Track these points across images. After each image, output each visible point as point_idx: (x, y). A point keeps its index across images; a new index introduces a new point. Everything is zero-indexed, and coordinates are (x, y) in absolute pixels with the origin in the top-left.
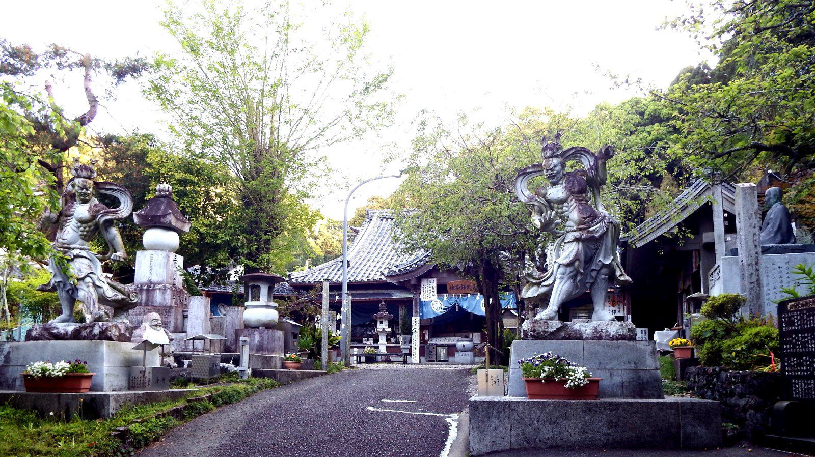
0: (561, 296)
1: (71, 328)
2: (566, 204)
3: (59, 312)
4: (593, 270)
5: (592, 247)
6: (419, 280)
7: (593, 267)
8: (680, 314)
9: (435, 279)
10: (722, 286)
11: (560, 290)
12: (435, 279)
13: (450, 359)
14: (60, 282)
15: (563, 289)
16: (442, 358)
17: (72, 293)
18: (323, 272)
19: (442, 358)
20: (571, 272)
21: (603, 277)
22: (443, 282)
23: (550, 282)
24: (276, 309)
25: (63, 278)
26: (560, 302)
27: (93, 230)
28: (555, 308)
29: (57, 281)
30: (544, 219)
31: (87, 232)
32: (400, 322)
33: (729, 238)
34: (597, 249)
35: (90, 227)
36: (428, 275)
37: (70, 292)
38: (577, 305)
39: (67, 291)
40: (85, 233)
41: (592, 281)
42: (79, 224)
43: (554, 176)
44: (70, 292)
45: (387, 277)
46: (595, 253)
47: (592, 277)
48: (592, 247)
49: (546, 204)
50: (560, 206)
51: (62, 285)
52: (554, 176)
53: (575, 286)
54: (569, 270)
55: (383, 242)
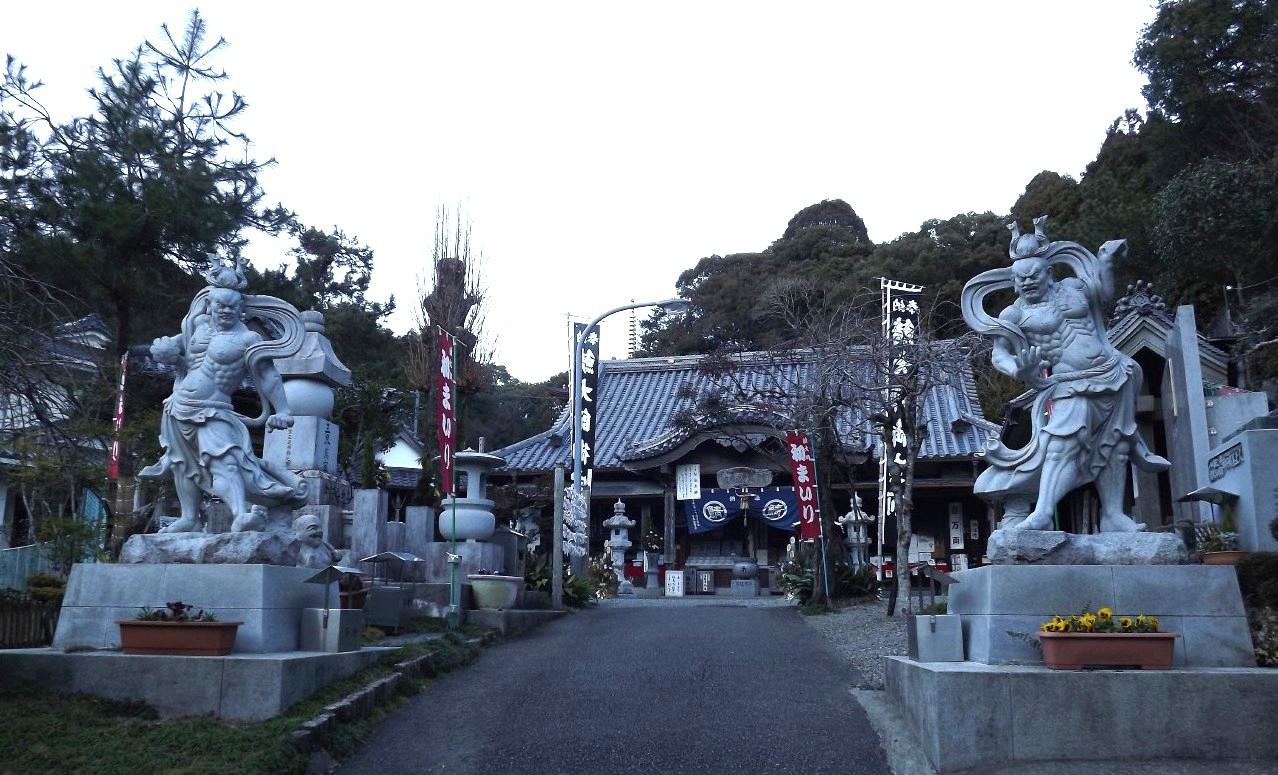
0: (1058, 489)
1: (199, 542)
2: (1056, 334)
3: (175, 512)
4: (1105, 445)
5: (1104, 406)
6: (673, 467)
7: (1104, 442)
8: (1073, 521)
9: (698, 466)
10: (1250, 477)
11: (1053, 482)
12: (698, 466)
13: (721, 590)
14: (180, 462)
15: (1061, 476)
16: (705, 588)
17: (200, 482)
18: (520, 453)
19: (705, 588)
20: (1073, 449)
21: (1121, 457)
22: (710, 470)
23: (1031, 466)
24: (493, 510)
25: (185, 455)
26: (1057, 499)
27: (239, 374)
28: (1050, 510)
29: (175, 460)
30: (1026, 360)
31: (229, 378)
32: (31, 519)
33: (1211, 403)
34: (1112, 411)
35: (234, 370)
36: (688, 460)
37: (197, 480)
38: (1078, 509)
39: (192, 479)
40: (225, 380)
41: (1102, 465)
42: (216, 365)
43: (1035, 288)
44: (197, 480)
45: (625, 462)
46: (1108, 419)
47: (1103, 458)
48: (1104, 406)
49: (1020, 333)
50: (1047, 337)
51: (183, 468)
52: (1035, 288)
53: (1079, 472)
54: (1069, 444)
55: (618, 410)
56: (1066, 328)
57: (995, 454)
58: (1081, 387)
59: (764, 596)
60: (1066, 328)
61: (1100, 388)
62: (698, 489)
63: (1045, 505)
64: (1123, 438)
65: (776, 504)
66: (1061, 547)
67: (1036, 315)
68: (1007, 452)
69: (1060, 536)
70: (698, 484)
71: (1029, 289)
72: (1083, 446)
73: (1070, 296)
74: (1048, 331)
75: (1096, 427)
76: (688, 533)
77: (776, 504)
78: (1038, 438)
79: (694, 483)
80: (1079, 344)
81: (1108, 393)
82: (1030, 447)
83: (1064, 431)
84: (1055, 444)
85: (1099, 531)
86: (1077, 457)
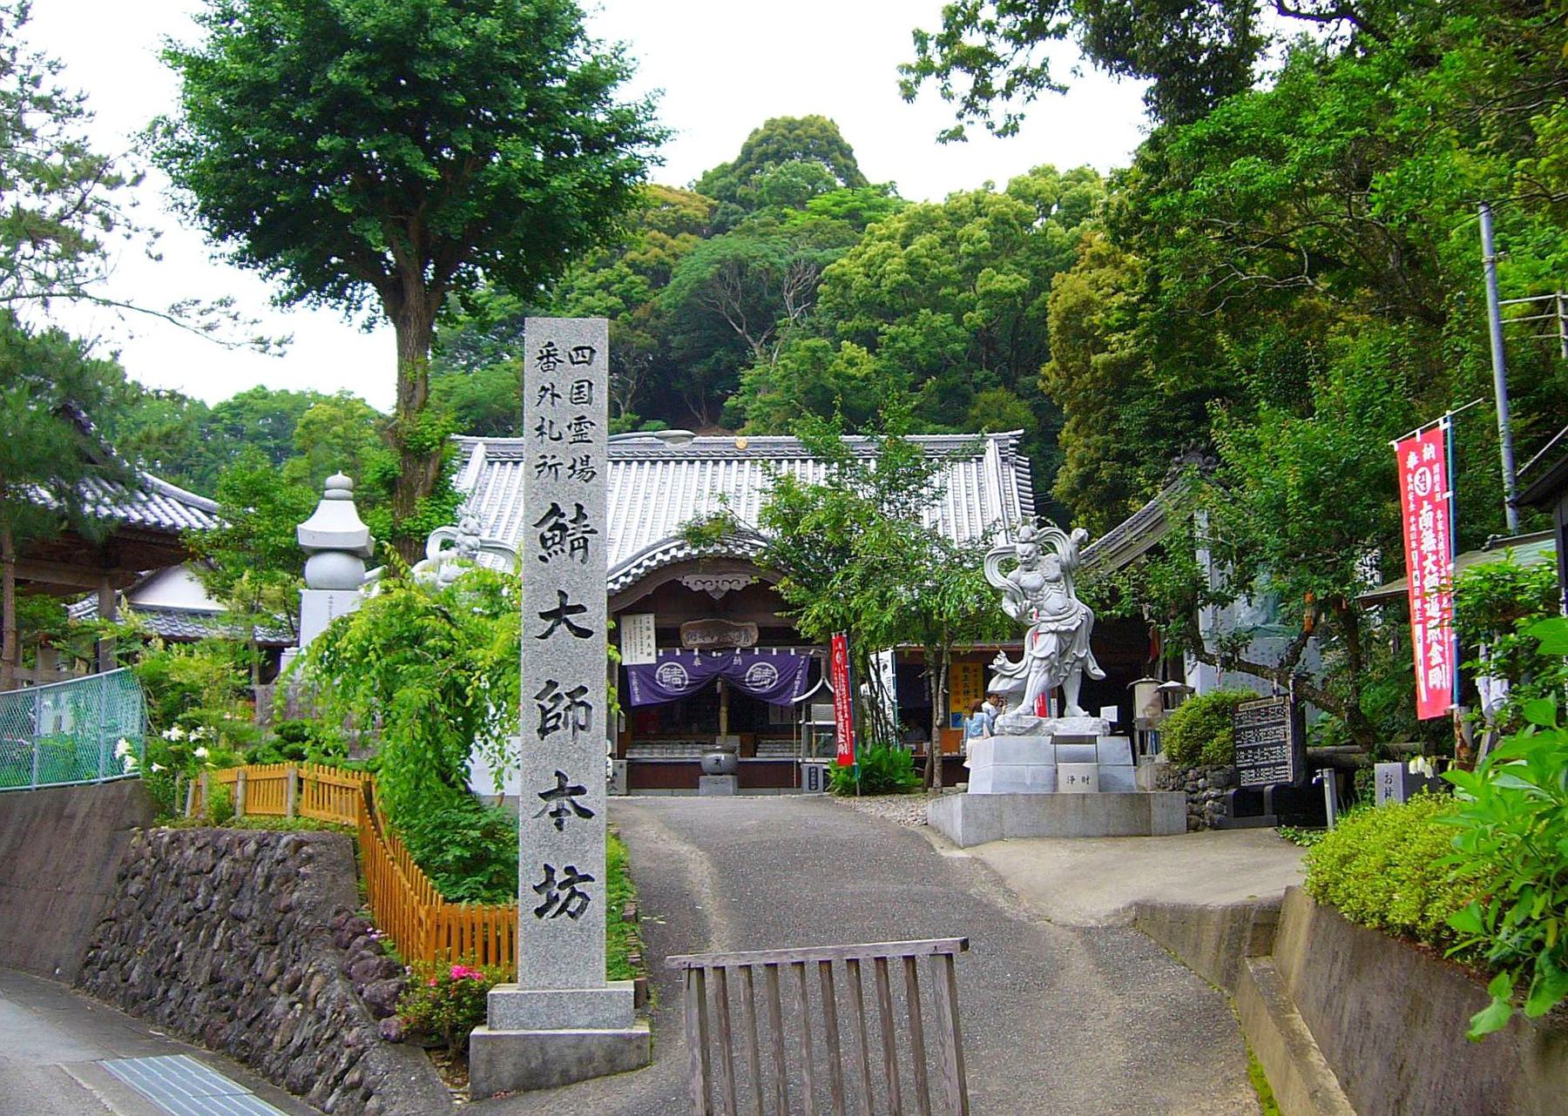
9: (652, 617)
12: (652, 617)
22: (668, 622)
53: (1050, 680)
56: (1046, 588)
57: (1001, 667)
58: (1053, 627)
59: (1168, 833)
60: (1046, 588)
61: (1063, 628)
62: (653, 649)
63: (1029, 700)
64: (1078, 659)
65: (764, 667)
66: (1036, 726)
67: (1030, 579)
68: (1010, 665)
69: (1035, 719)
70: (653, 642)
71: (1025, 563)
72: (1052, 664)
73: (1050, 566)
74: (1036, 590)
75: (1062, 653)
76: (89, 545)
77: (764, 667)
78: (1027, 658)
79: (646, 633)
80: (1055, 598)
81: (1068, 631)
82: (1022, 663)
83: (1042, 655)
84: (1036, 662)
85: (1061, 715)
86: (1049, 671)
